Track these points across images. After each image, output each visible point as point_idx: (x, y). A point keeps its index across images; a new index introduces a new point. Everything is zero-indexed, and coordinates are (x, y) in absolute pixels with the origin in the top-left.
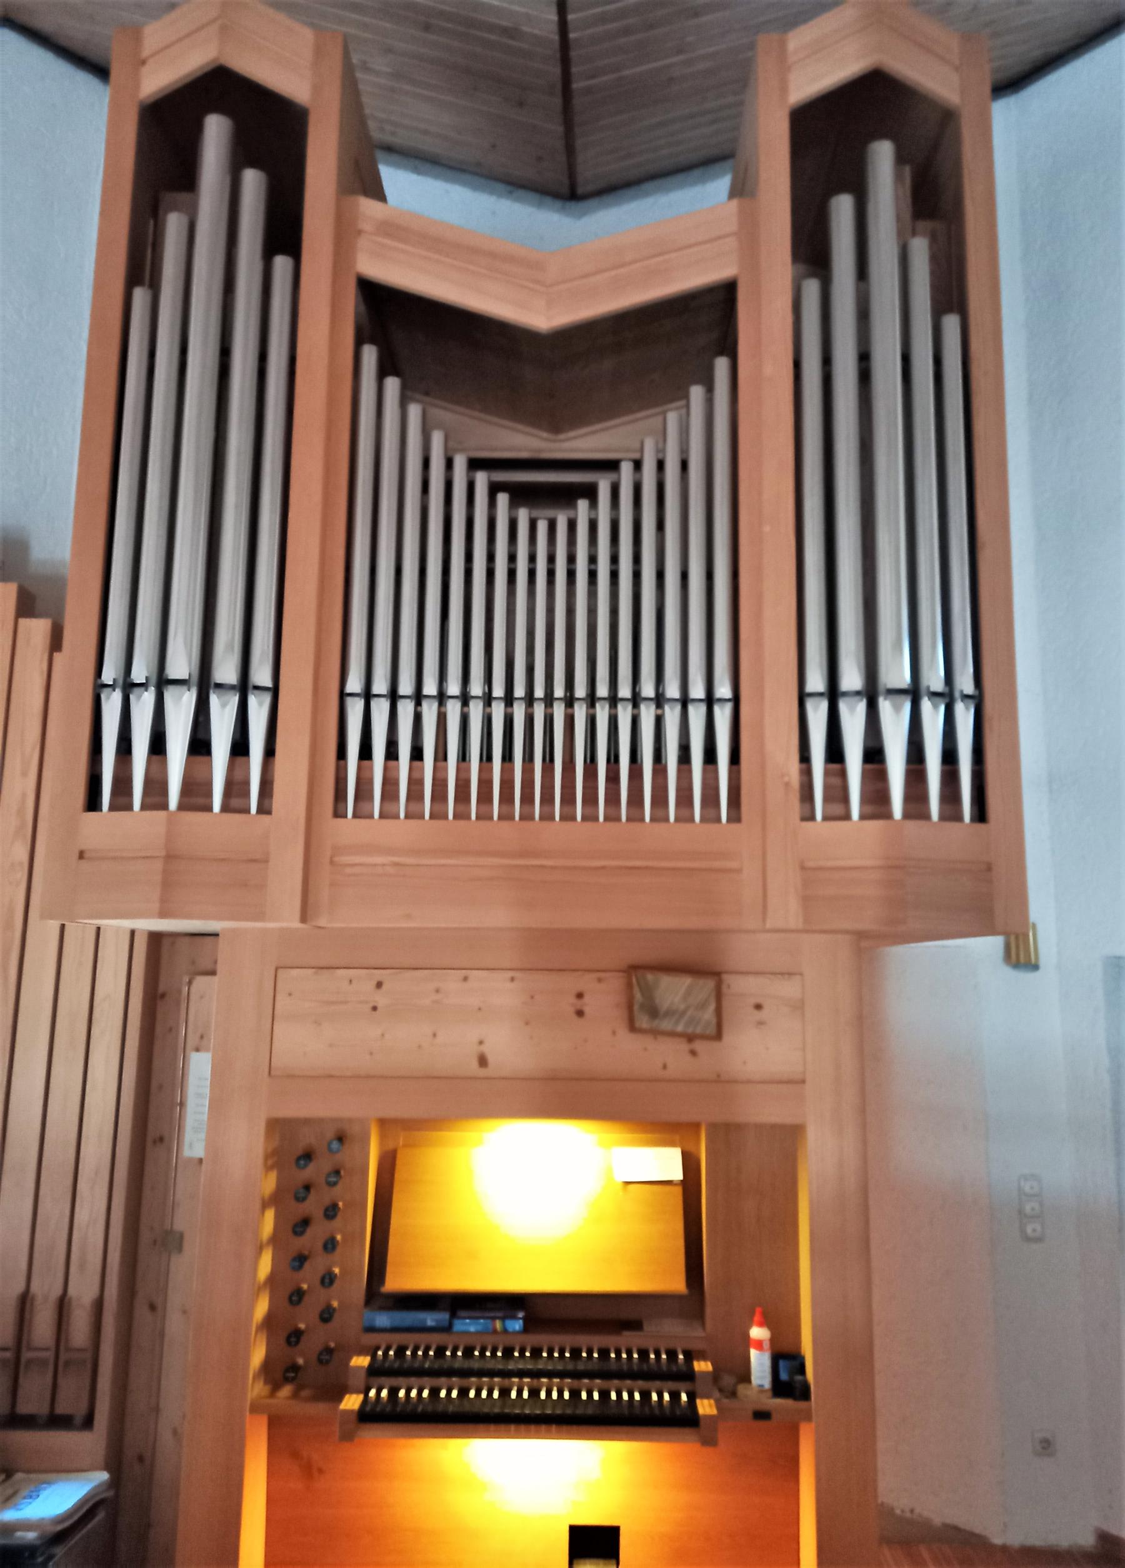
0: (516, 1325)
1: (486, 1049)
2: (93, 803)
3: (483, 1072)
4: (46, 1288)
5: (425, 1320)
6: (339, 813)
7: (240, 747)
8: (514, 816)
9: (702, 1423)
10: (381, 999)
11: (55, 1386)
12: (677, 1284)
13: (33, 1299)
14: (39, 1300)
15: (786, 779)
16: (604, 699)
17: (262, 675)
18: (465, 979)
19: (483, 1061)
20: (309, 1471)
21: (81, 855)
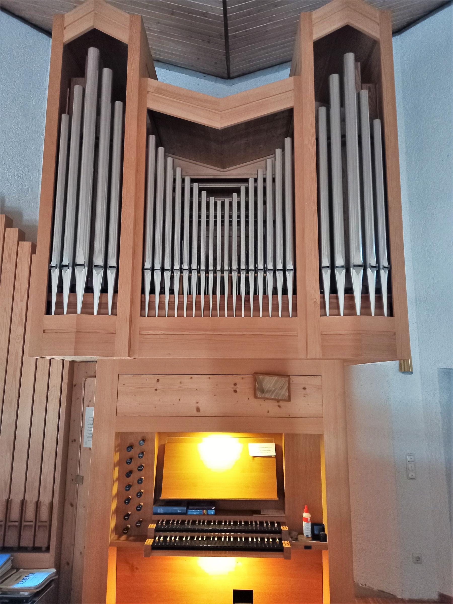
2: (48, 312)
3: (198, 414)
5: (177, 510)
7: (104, 290)
9: (285, 550)
10: (159, 386)
14: (28, 503)
15: (315, 300)
18: (191, 378)
19: (198, 410)
21: (44, 332)
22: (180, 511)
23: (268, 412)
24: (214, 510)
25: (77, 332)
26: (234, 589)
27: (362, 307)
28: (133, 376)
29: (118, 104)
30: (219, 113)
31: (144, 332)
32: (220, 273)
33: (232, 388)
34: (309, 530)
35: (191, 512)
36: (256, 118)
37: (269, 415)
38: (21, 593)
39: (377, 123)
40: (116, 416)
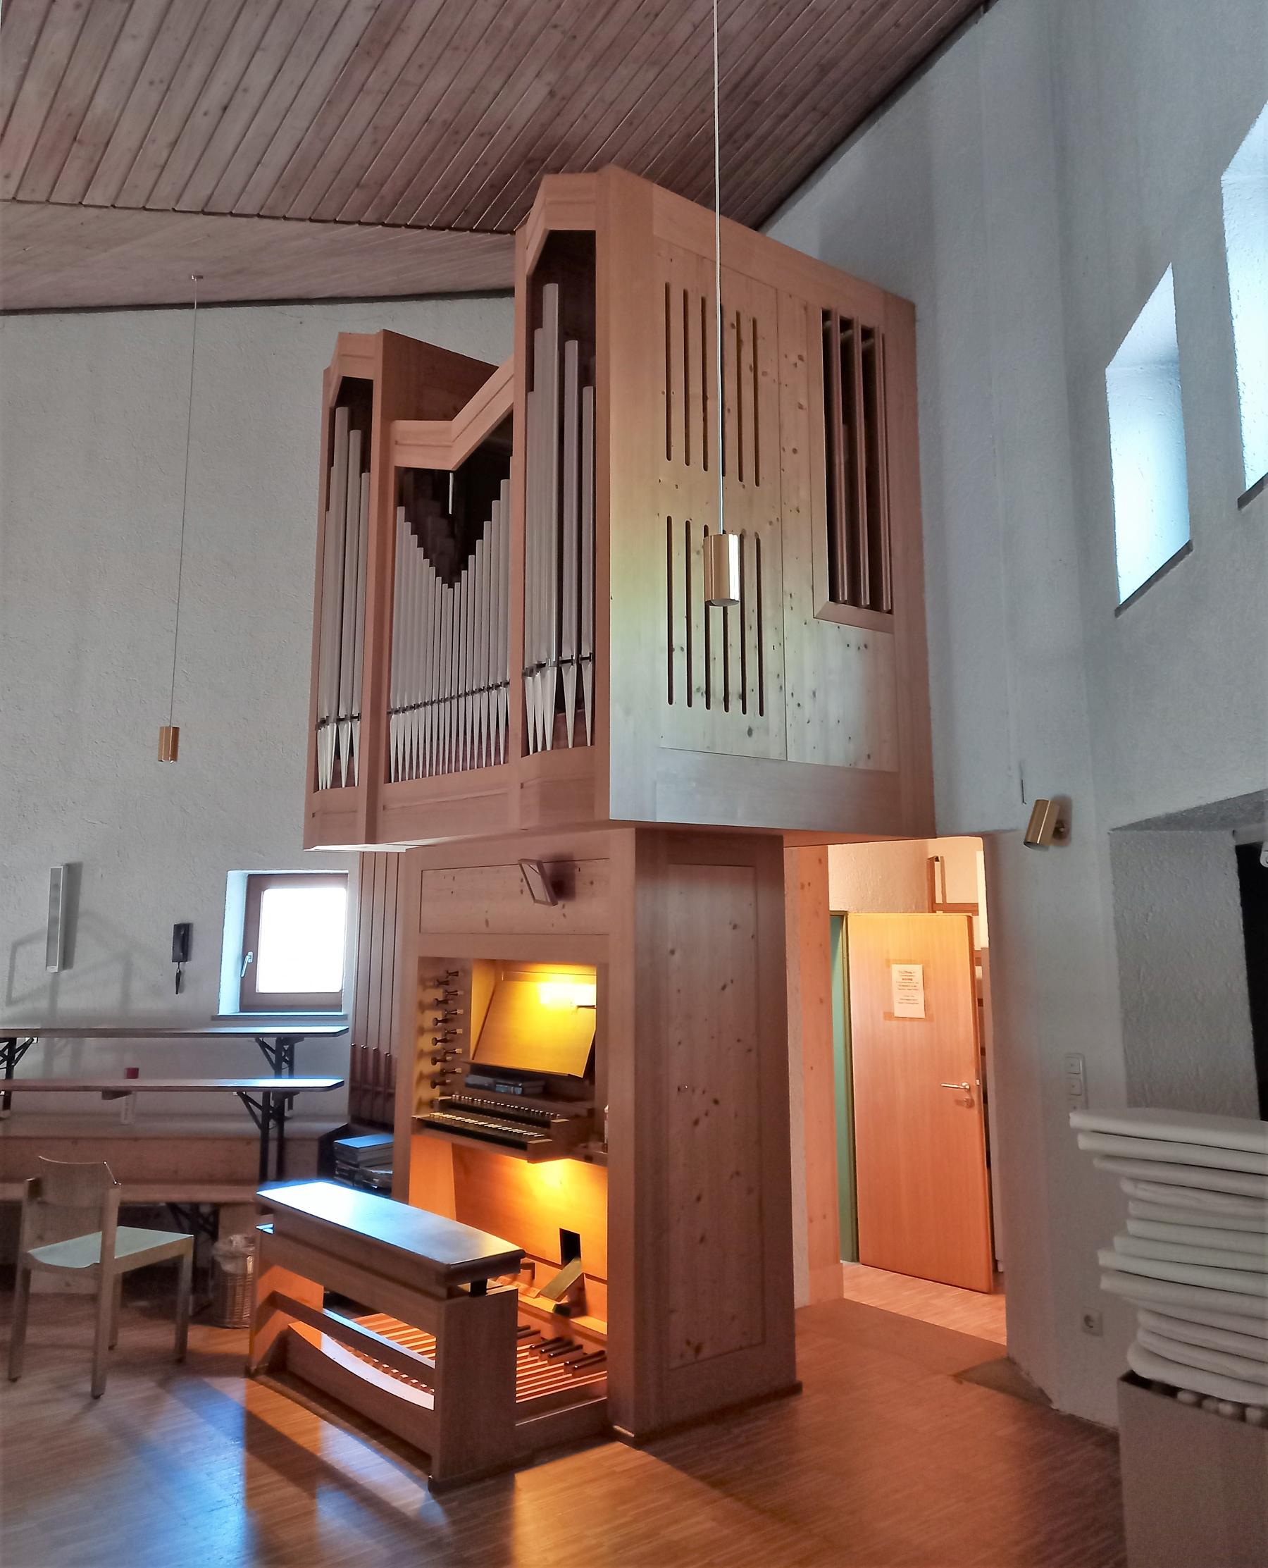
12: (579, 1072)
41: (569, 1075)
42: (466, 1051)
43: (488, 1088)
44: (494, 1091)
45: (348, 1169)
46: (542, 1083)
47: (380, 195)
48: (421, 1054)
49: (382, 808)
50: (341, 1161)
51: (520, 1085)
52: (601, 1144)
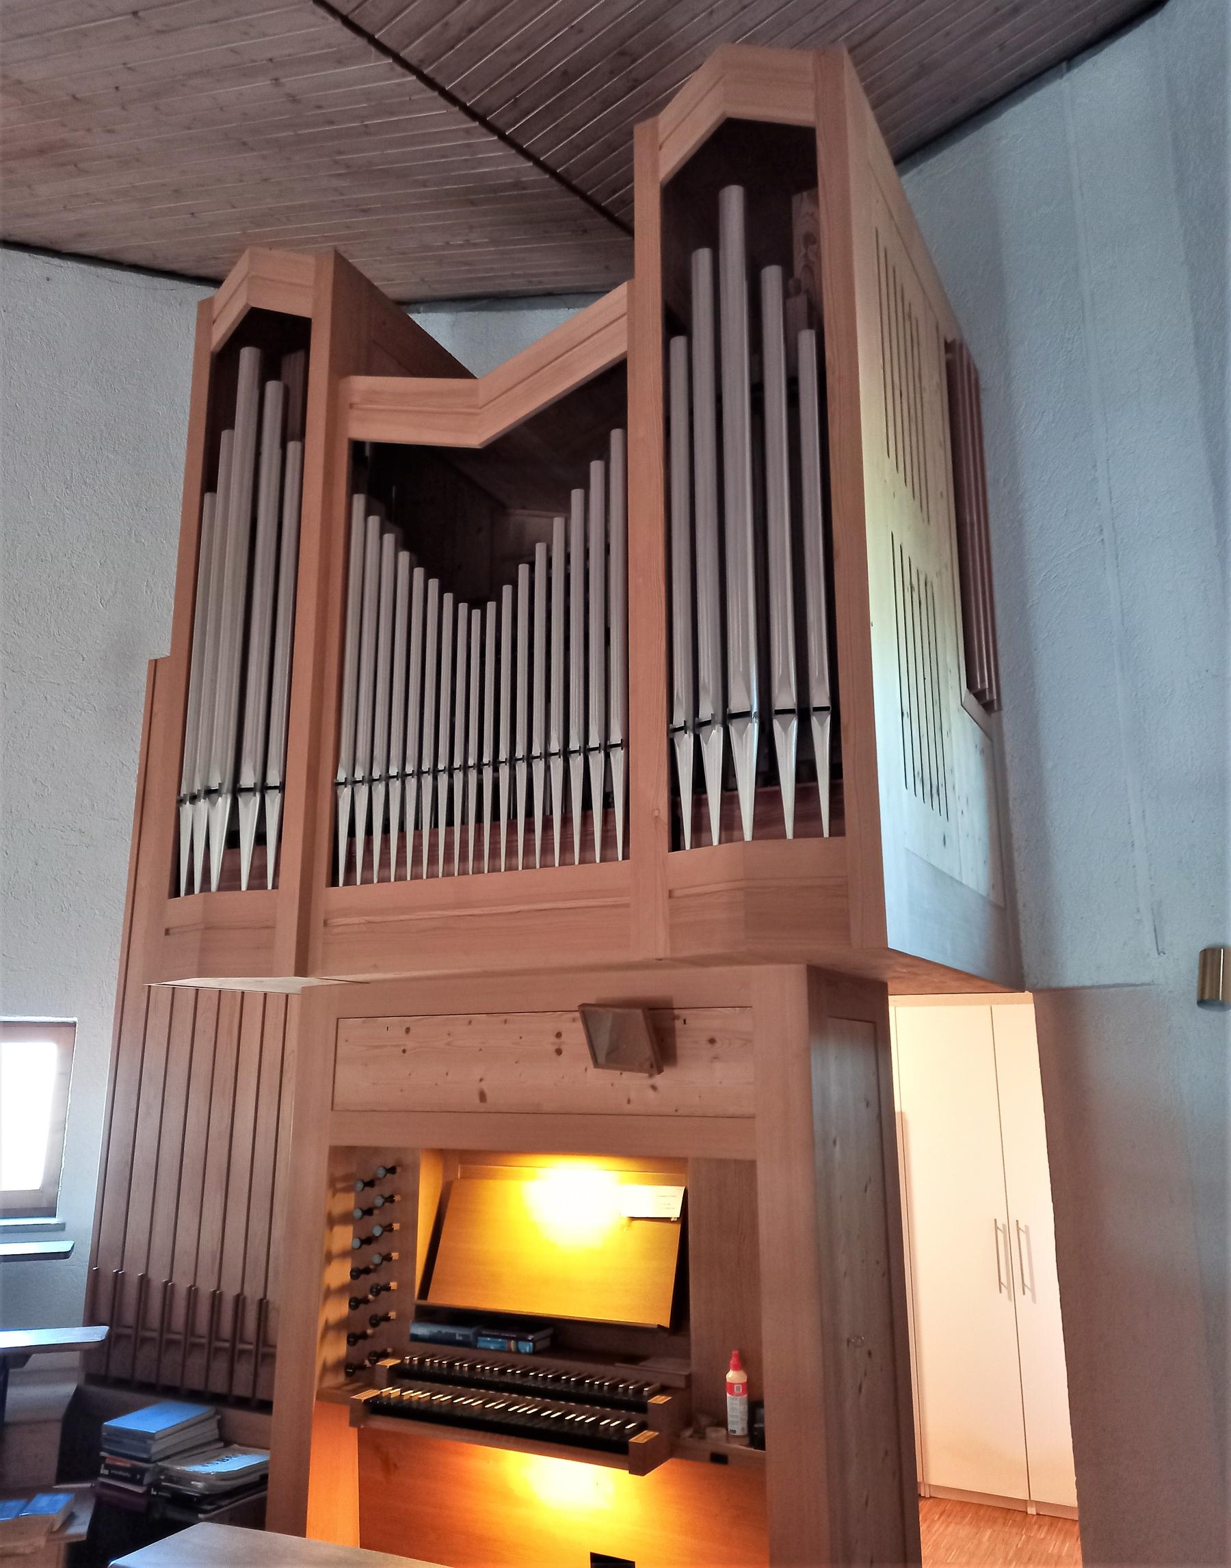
0: (527, 1347)
1: (484, 1086)
2: (176, 893)
3: (483, 1107)
4: (230, 1291)
5: (455, 1335)
6: (334, 882)
7: (260, 839)
8: (390, 879)
9: (631, 1451)
10: (410, 1044)
11: (256, 1375)
12: (662, 1318)
13: (245, 1299)
14: (249, 1301)
15: (656, 813)
16: (275, 788)
17: (820, 697)
18: (505, 1022)
19: (482, 1097)
20: (388, 1466)
21: (167, 932)
22: (461, 1338)
23: (629, 1101)
24: (531, 1344)
25: (206, 928)
26: (593, 1552)
27: (798, 818)
28: (364, 1022)
29: (293, 447)
30: (478, 411)
31: (338, 920)
32: (462, 776)
33: (553, 1044)
34: (737, 1417)
35: (484, 1341)
36: (556, 400)
37: (628, 1108)
38: (192, 1483)
39: (807, 340)
40: (332, 1109)
41: (659, 1326)
42: (406, 1285)
43: (463, 1344)
44: (476, 1348)
45: (128, 1465)
46: (549, 1331)
47: (445, 20)
48: (328, 1293)
49: (322, 923)
50: (111, 1453)
51: (530, 1338)
52: (724, 1431)
